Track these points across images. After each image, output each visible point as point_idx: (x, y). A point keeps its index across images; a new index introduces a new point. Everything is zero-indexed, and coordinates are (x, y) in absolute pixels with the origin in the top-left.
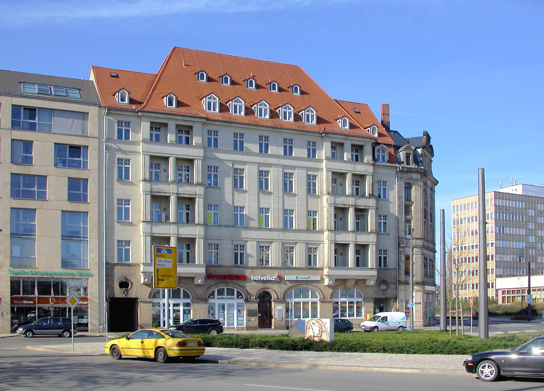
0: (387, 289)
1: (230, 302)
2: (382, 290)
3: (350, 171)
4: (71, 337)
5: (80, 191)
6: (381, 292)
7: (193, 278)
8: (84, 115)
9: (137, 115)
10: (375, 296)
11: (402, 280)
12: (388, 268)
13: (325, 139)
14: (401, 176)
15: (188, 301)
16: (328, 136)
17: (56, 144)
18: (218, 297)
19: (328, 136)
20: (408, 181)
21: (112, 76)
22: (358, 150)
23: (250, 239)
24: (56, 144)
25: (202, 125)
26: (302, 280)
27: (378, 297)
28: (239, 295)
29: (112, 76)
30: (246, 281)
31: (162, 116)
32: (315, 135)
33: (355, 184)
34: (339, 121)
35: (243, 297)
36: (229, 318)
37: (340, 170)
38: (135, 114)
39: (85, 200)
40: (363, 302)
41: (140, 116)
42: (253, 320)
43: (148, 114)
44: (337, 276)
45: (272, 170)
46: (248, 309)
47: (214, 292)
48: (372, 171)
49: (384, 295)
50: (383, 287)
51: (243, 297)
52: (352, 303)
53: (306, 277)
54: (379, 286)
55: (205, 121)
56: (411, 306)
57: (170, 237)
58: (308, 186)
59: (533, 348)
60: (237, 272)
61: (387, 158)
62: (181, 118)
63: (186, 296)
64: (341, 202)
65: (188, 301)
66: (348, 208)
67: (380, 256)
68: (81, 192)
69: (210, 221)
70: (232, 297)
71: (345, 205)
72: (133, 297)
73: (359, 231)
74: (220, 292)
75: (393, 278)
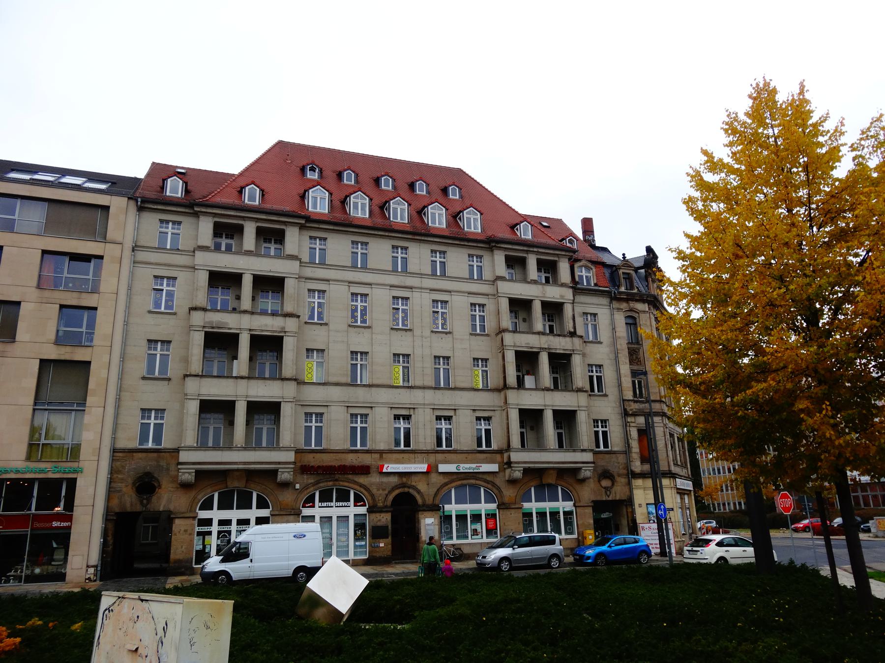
0: (613, 484)
1: (343, 512)
3: (537, 297)
4: (550, 512)
6: (603, 490)
7: (275, 472)
9: (192, 211)
10: (593, 498)
11: (636, 470)
12: (611, 451)
14: (619, 307)
15: (265, 513)
16: (499, 245)
18: (320, 505)
19: (499, 245)
20: (629, 314)
22: (561, 424)
23: (378, 403)
26: (466, 471)
27: (599, 498)
28: (358, 500)
30: (370, 475)
33: (547, 320)
34: (517, 229)
35: (364, 502)
36: (345, 544)
40: (497, 510)
42: (382, 545)
45: (415, 296)
46: (372, 524)
47: (314, 495)
48: (572, 298)
49: (608, 497)
50: (606, 483)
51: (364, 505)
52: (228, 522)
53: (474, 466)
54: (599, 481)
56: (663, 513)
58: (472, 321)
59: (798, 566)
60: (355, 461)
61: (593, 280)
63: (262, 505)
64: (526, 344)
65: (265, 513)
66: (538, 353)
68: (84, 329)
69: (309, 376)
70: (329, 504)
71: (531, 348)
73: (549, 283)
74: (326, 497)
75: (621, 467)
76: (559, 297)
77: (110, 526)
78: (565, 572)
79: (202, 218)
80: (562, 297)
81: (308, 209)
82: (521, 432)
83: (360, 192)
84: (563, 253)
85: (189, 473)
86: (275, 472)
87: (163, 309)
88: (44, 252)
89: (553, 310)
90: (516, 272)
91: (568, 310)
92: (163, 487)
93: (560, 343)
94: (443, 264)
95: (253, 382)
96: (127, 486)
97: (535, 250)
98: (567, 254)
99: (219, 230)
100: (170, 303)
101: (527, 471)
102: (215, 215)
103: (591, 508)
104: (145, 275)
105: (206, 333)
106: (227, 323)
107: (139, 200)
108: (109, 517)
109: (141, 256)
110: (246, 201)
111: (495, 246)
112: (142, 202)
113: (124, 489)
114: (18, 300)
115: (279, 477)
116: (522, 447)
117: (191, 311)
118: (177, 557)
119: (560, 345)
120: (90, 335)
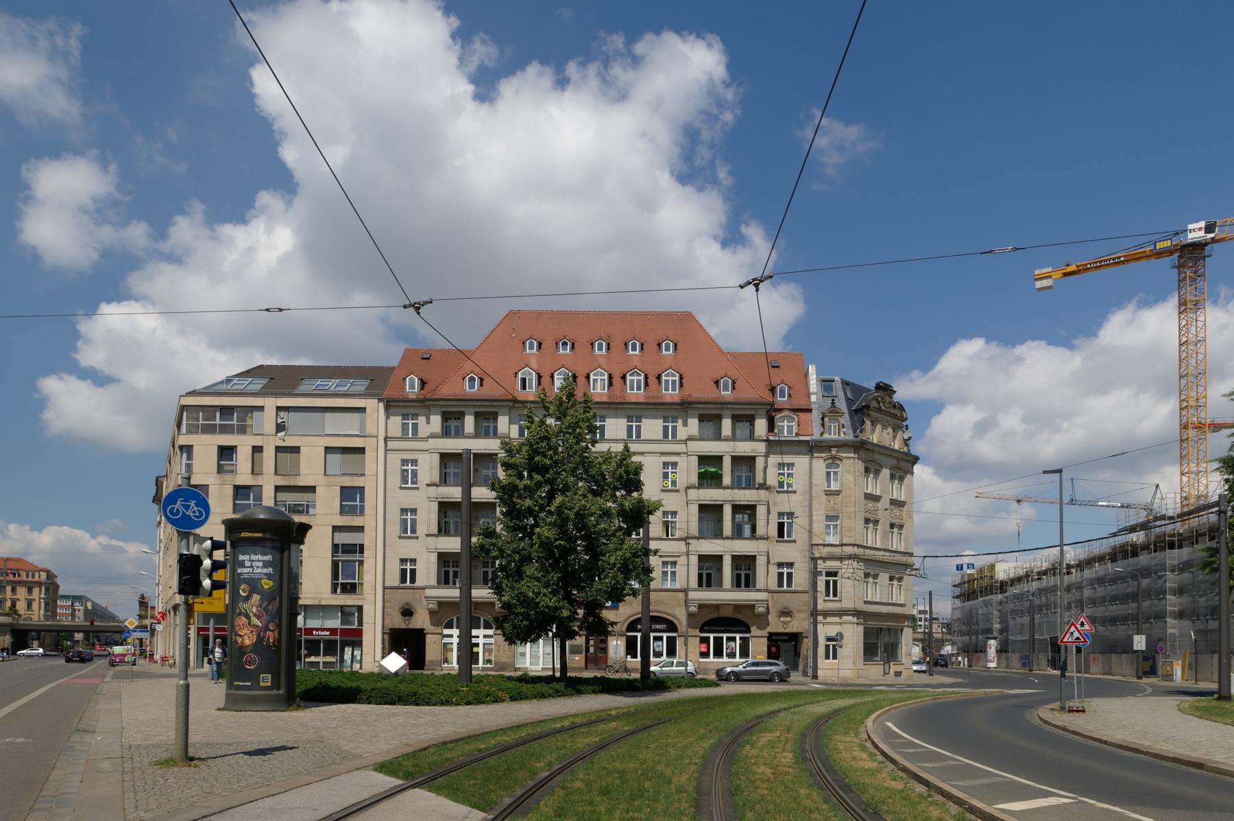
2: (782, 622)
5: (356, 501)
7: (753, 607)
8: (362, 410)
13: (690, 412)
17: (219, 446)
21: (423, 358)
24: (219, 446)
25: (510, 409)
29: (423, 358)
31: (454, 403)
32: (673, 407)
37: (745, 452)
38: (421, 404)
39: (362, 513)
41: (427, 406)
42: (577, 658)
43: (437, 403)
44: (700, 600)
45: (422, 458)
49: (785, 629)
55: (511, 404)
57: (721, 556)
62: (479, 403)
67: (738, 572)
68: (358, 503)
72: (418, 627)
73: (450, 434)
76: (750, 451)
77: (386, 637)
78: (815, 689)
79: (433, 409)
80: (753, 451)
81: (465, 390)
82: (699, 573)
83: (563, 369)
84: (760, 407)
85: (433, 604)
86: (753, 607)
87: (410, 485)
88: (326, 448)
89: (744, 462)
90: (710, 428)
91: (760, 462)
92: (418, 612)
93: (745, 495)
94: (639, 428)
95: (702, 541)
96: (395, 611)
97: (729, 406)
98: (764, 407)
99: (446, 417)
100: (415, 479)
101: (701, 606)
102: (475, 406)
103: (766, 639)
104: (395, 459)
105: (439, 503)
106: (454, 494)
107: (385, 401)
108: (385, 631)
109: (391, 445)
110: (467, 389)
111: (687, 407)
112: (387, 402)
113: (394, 613)
114: (314, 485)
115: (756, 610)
116: (438, 584)
117: (688, 491)
118: (430, 659)
119: (744, 497)
120: (362, 508)
